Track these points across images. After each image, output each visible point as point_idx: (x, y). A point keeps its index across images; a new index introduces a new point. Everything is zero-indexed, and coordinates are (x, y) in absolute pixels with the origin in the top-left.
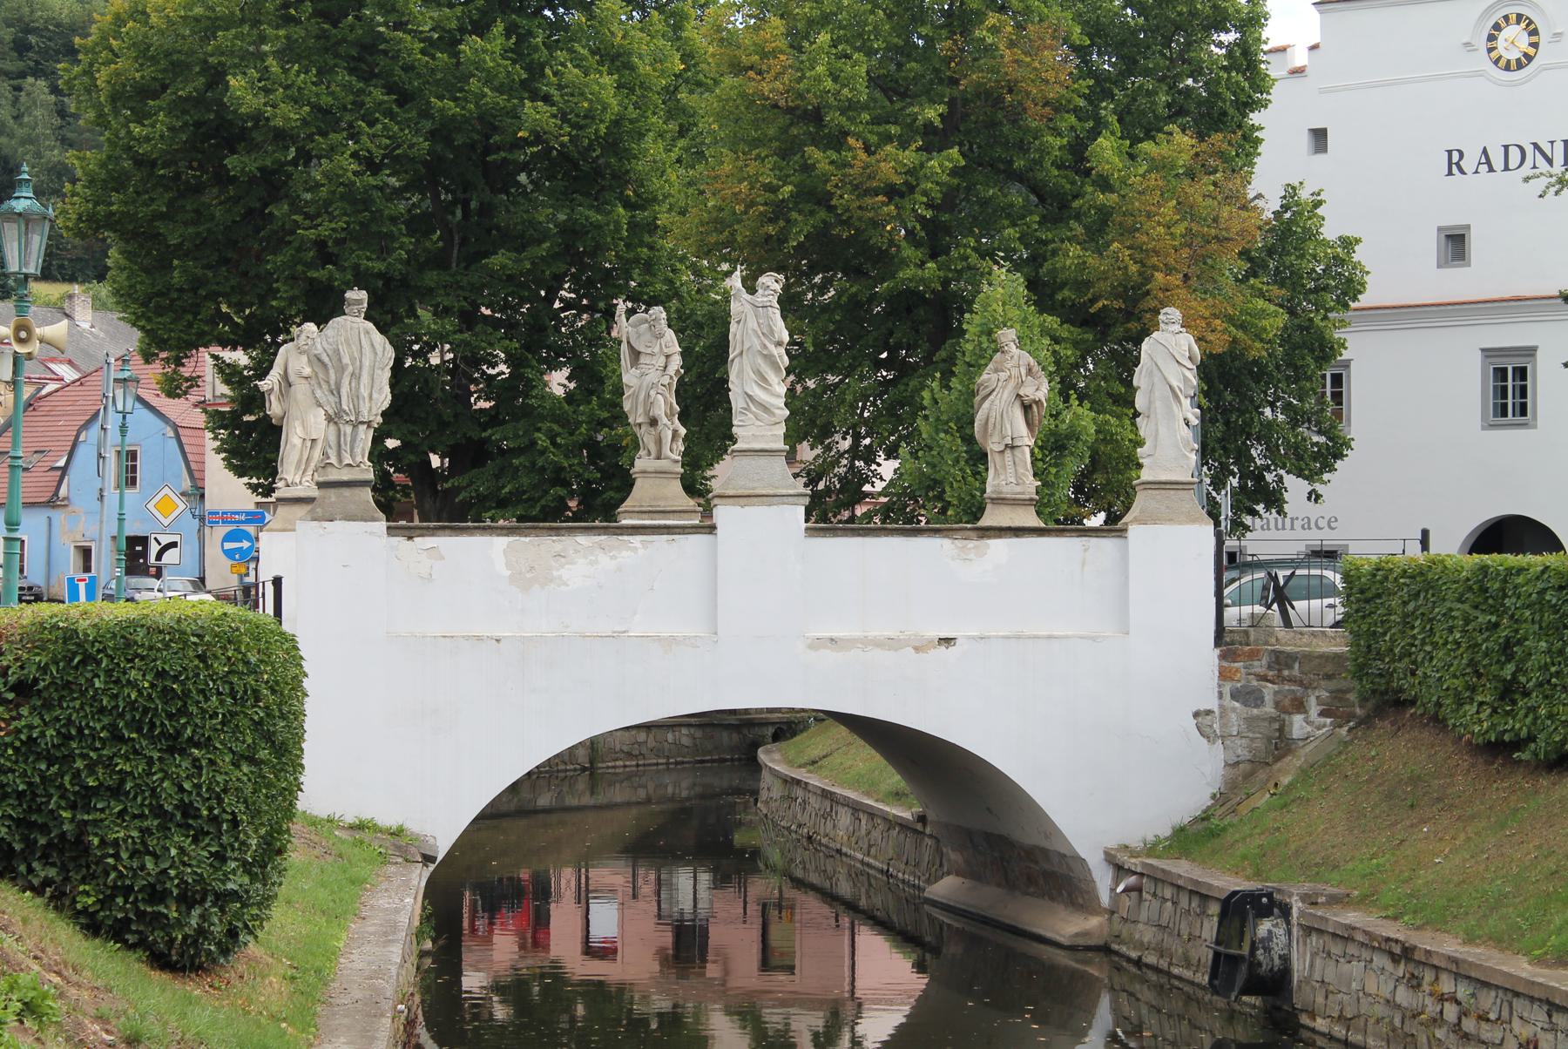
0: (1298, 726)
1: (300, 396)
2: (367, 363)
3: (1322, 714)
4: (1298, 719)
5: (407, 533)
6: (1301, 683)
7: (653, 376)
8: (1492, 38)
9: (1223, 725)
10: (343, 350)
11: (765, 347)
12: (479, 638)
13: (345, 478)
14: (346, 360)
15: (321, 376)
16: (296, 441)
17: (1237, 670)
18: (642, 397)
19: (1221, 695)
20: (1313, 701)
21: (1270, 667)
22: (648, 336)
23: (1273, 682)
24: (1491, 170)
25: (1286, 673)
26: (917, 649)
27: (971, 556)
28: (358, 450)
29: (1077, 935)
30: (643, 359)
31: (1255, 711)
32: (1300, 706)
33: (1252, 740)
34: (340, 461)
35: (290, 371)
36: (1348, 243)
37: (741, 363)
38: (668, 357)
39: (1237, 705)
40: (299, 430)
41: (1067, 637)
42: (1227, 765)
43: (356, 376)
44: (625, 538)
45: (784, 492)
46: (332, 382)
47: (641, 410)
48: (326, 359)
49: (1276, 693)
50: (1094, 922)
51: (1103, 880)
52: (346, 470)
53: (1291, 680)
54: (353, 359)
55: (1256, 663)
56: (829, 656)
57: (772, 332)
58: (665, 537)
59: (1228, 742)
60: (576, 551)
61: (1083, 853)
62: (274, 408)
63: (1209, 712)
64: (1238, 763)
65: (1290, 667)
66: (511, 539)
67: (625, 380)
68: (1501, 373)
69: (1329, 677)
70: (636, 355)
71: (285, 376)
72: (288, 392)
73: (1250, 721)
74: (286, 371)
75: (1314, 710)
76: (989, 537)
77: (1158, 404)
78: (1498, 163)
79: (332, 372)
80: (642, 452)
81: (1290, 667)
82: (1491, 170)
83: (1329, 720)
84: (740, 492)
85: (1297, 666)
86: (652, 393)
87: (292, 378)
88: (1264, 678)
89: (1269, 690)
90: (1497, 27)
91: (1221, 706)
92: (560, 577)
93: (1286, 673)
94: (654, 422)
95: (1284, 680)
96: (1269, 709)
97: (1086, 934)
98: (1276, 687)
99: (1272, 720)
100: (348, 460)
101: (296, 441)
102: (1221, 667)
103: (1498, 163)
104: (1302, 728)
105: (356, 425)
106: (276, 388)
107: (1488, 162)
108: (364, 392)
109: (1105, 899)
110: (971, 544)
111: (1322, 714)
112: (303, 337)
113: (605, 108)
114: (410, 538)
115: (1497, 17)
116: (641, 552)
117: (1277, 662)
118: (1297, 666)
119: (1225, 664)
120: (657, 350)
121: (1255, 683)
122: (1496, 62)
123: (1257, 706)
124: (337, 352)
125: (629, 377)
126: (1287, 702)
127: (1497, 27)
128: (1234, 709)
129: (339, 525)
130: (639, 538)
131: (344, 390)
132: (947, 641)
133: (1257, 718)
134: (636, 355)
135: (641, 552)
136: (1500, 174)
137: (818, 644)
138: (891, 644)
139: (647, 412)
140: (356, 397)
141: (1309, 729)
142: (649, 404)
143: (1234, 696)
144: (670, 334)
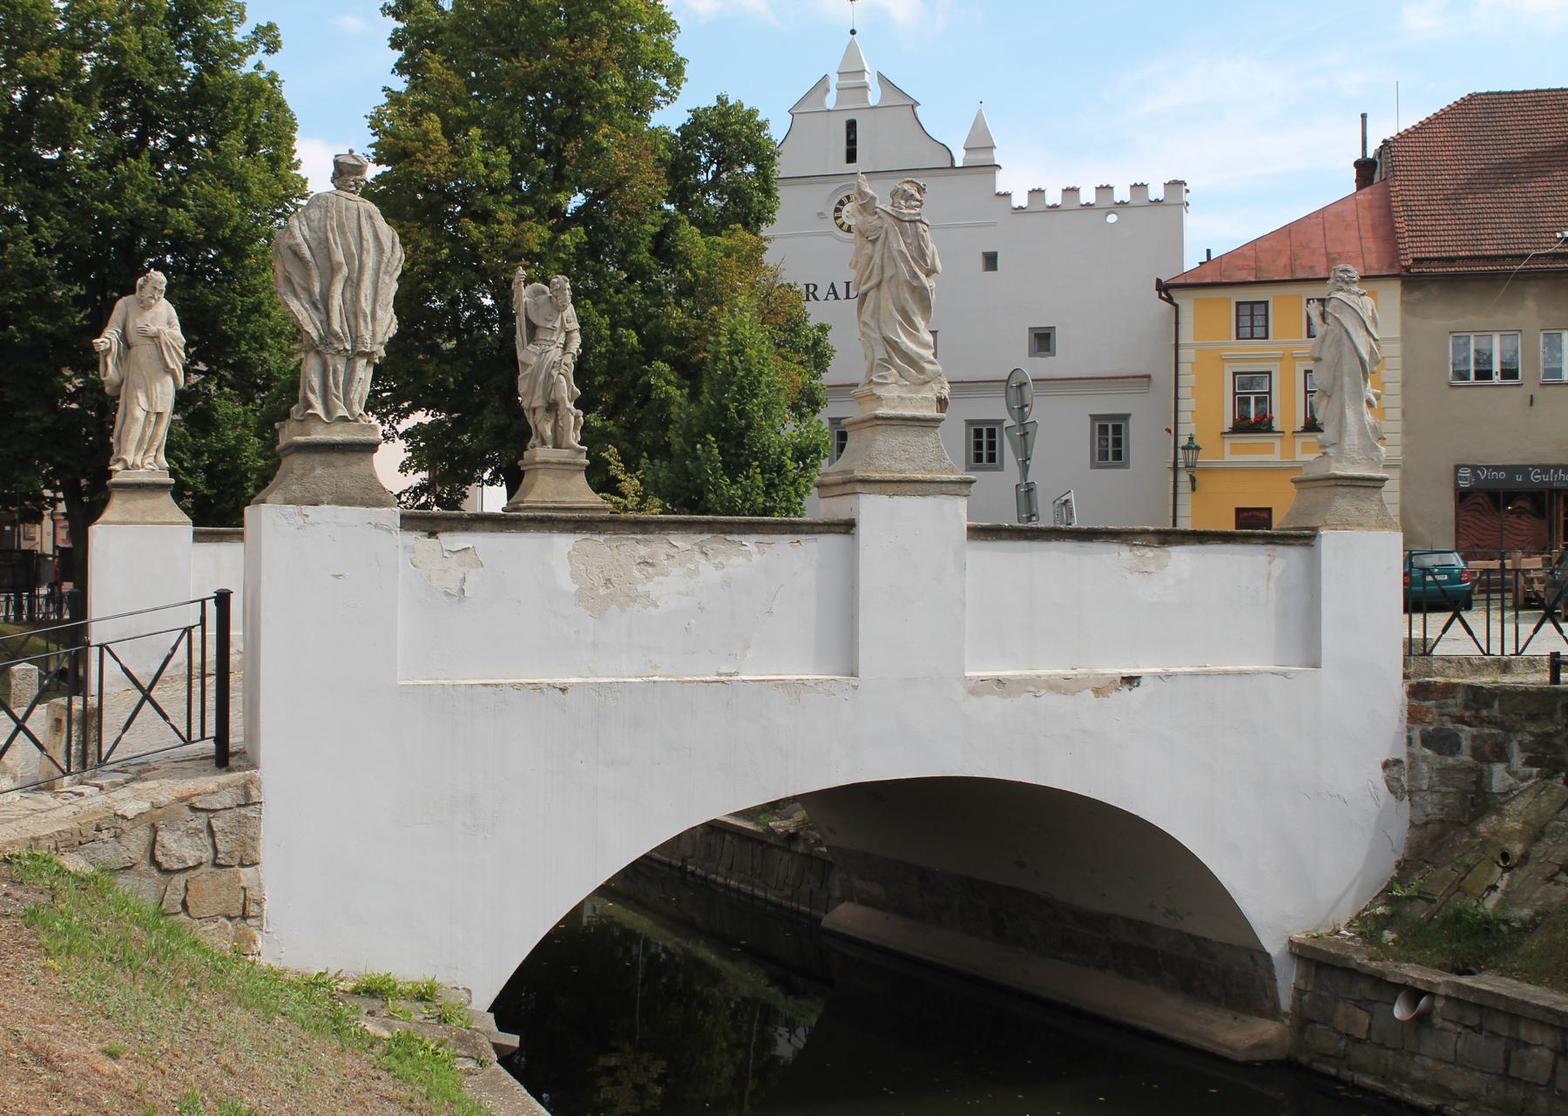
0: (1499, 777)
1: (143, 360)
2: (370, 262)
3: (1529, 762)
4: (1498, 769)
5: (429, 526)
6: (1501, 725)
7: (555, 354)
8: (837, 210)
9: (1412, 778)
10: (335, 240)
11: (915, 276)
12: (536, 687)
13: (338, 438)
14: (339, 256)
15: (296, 279)
16: (140, 414)
17: (1428, 710)
18: (542, 377)
19: (1410, 741)
20: (1515, 747)
21: (1466, 707)
22: (548, 309)
23: (1470, 725)
24: (837, 298)
25: (1484, 713)
26: (1098, 692)
27: (1152, 568)
28: (355, 397)
29: (1253, 1047)
30: (541, 335)
31: (1450, 760)
32: (1501, 755)
33: (1444, 794)
34: (328, 412)
35: (130, 326)
36: (823, 329)
37: (878, 299)
38: (568, 334)
39: (1429, 752)
40: (142, 399)
41: (1258, 673)
42: (1413, 825)
43: (353, 284)
44: (736, 537)
45: (945, 477)
46: (317, 289)
47: (539, 392)
48: (308, 254)
49: (1474, 738)
50: (1268, 1030)
51: (1287, 980)
52: (338, 427)
53: (1490, 722)
54: (348, 256)
55: (1450, 701)
56: (995, 704)
57: (923, 255)
58: (788, 537)
59: (1417, 798)
60: (669, 557)
61: (1268, 949)
62: (110, 372)
63: (1397, 762)
64: (1427, 823)
65: (1489, 706)
66: (579, 537)
67: (521, 356)
68: (978, 433)
69: (1533, 718)
70: (532, 329)
71: (124, 337)
72: (126, 355)
73: (1444, 772)
74: (124, 329)
75: (1517, 759)
76: (1171, 544)
77: (1346, 380)
78: (841, 292)
79: (315, 273)
80: (533, 441)
81: (1489, 706)
82: (837, 298)
83: (1535, 770)
84: (888, 476)
85: (1496, 705)
86: (555, 373)
87: (133, 337)
88: (1460, 720)
89: (1466, 733)
90: (841, 203)
91: (1410, 755)
92: (647, 595)
93: (1484, 713)
94: (552, 407)
95: (1483, 722)
96: (1465, 757)
97: (1264, 1046)
98: (1474, 731)
99: (1470, 770)
100: (342, 411)
101: (140, 414)
102: (1410, 706)
103: (841, 292)
104: (1503, 779)
105: (351, 358)
106: (115, 348)
107: (835, 293)
108: (366, 306)
109: (1285, 1000)
110: (1149, 553)
111: (1529, 762)
112: (148, 288)
113: (231, 216)
114: (432, 534)
115: (842, 196)
116: (756, 558)
117: (1475, 700)
118: (1496, 705)
119: (1415, 703)
120: (558, 324)
121: (1449, 726)
122: (841, 227)
123: (1452, 754)
124: (325, 244)
125: (527, 354)
126: (1487, 749)
127: (841, 203)
128: (1425, 758)
129: (327, 511)
130: (754, 538)
131: (336, 301)
132: (1131, 681)
133: (1453, 768)
134: (532, 329)
135: (756, 558)
136: (843, 302)
137: (980, 687)
138: (1057, 686)
139: (547, 395)
140: (353, 313)
141: (1511, 780)
142: (550, 385)
143: (1426, 742)
144: (570, 310)
